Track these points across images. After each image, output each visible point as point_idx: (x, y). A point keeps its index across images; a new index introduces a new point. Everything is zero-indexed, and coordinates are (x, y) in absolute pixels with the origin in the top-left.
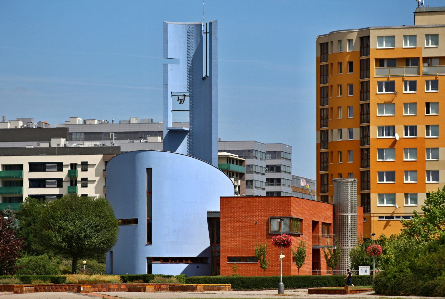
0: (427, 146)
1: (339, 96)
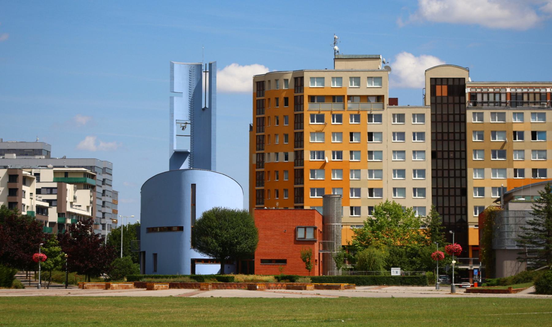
0: (351, 168)
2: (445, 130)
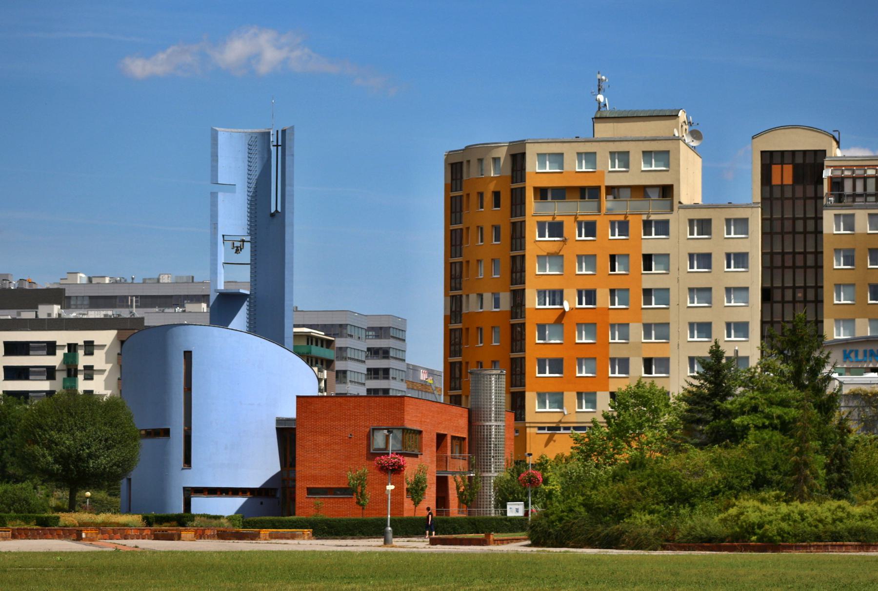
0: (611, 321)
2: (788, 249)
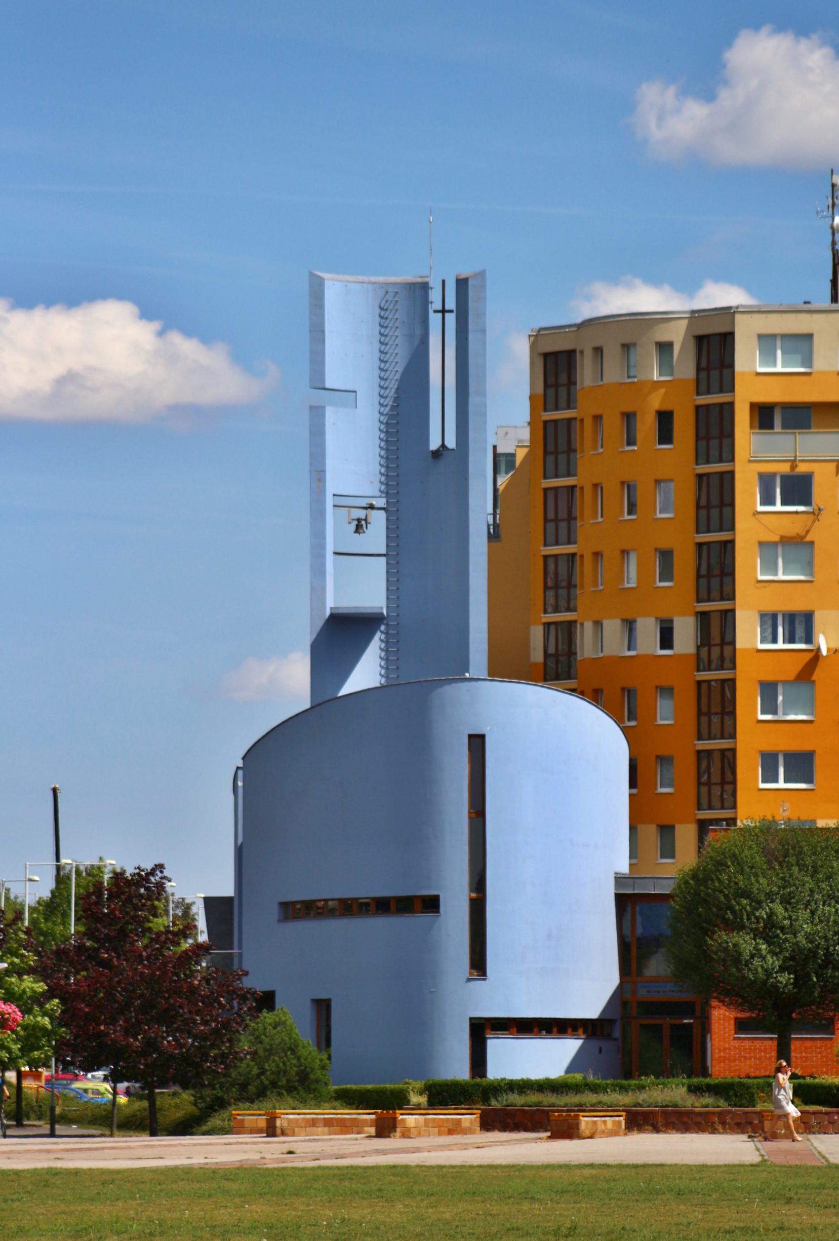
1: (624, 516)
